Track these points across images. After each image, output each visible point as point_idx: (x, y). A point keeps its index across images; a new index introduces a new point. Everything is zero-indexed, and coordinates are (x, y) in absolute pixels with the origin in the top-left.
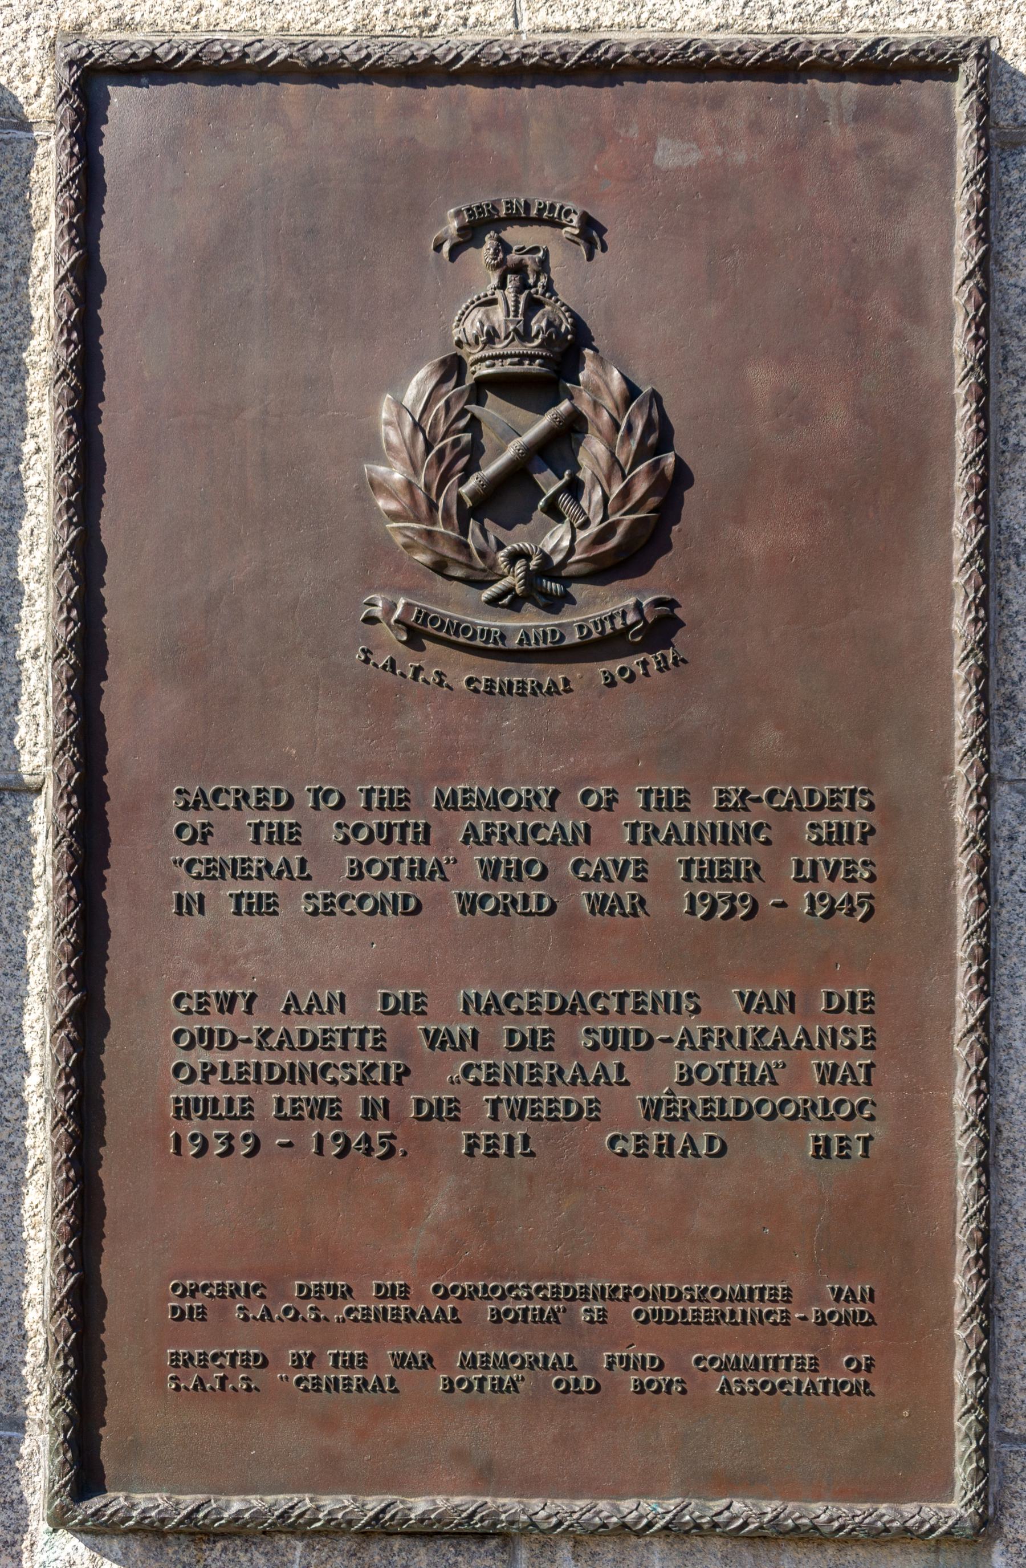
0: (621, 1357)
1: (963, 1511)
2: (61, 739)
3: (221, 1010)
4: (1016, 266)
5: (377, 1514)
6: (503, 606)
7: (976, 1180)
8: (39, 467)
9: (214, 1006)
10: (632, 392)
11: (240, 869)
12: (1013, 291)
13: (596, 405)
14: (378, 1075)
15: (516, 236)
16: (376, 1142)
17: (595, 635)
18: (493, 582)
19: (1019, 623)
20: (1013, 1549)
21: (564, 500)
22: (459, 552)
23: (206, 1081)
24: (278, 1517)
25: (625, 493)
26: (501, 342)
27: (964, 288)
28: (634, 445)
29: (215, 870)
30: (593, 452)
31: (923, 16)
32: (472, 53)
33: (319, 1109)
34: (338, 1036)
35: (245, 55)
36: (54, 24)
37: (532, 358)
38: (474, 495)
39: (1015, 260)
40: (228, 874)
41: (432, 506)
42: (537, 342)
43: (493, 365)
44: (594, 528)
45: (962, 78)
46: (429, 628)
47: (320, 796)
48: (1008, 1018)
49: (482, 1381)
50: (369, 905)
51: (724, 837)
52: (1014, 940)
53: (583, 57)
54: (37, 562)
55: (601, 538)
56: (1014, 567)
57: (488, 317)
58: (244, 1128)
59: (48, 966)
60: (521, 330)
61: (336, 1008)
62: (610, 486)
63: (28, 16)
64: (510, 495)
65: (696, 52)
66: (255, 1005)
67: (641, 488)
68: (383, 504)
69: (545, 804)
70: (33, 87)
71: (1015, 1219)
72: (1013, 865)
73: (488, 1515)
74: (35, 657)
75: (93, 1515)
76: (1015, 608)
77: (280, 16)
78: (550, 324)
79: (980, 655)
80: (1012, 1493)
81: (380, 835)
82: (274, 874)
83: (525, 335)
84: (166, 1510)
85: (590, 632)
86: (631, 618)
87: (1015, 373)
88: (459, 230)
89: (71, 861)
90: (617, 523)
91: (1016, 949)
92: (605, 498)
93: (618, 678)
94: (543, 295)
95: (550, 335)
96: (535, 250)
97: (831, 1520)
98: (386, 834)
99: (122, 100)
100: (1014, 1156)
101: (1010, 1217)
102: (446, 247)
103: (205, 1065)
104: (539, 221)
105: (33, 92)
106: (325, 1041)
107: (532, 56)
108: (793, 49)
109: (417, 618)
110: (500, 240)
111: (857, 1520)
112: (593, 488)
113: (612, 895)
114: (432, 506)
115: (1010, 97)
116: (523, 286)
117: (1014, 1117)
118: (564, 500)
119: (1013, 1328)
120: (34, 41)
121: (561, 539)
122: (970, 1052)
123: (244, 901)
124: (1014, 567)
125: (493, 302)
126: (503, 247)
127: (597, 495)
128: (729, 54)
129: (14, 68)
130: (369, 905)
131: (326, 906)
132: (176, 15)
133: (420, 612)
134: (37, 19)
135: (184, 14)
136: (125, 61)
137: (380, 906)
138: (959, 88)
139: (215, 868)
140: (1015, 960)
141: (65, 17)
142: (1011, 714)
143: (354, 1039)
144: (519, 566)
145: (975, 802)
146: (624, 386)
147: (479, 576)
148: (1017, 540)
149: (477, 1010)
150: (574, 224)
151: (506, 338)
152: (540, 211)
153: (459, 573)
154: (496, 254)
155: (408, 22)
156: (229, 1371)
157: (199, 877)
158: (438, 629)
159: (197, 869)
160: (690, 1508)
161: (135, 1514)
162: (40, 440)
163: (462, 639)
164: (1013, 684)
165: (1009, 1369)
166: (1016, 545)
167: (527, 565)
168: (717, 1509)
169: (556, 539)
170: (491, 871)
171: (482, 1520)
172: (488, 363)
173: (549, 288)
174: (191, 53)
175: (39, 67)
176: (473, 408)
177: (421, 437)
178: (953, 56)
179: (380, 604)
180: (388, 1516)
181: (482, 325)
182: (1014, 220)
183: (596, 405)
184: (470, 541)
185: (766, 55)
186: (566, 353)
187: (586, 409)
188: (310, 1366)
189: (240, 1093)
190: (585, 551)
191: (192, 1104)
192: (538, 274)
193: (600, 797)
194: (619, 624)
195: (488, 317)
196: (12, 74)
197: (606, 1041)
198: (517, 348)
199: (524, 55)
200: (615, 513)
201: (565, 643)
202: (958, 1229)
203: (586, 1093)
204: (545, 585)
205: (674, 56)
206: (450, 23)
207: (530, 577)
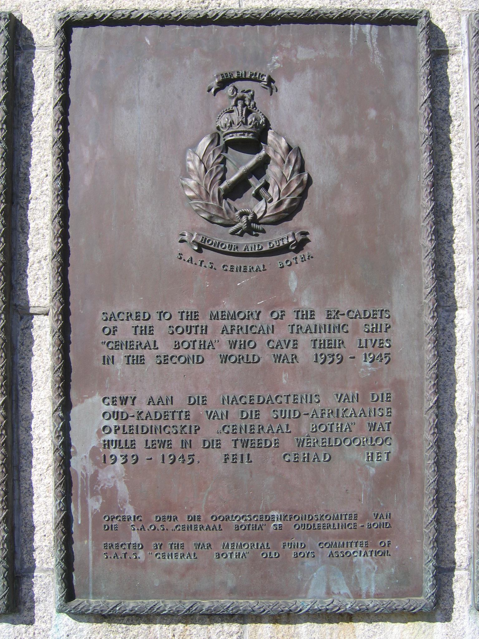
0: (289, 543)
1: (427, 601)
2: (55, 292)
3: (122, 404)
4: (440, 101)
5: (190, 608)
6: (237, 235)
7: (433, 469)
8: (47, 183)
9: (119, 402)
10: (289, 148)
11: (129, 345)
12: (439, 111)
13: (275, 152)
14: (187, 430)
15: (238, 84)
16: (186, 457)
17: (275, 247)
18: (233, 225)
19: (445, 243)
20: (444, 612)
21: (262, 191)
22: (219, 213)
23: (116, 433)
24: (149, 609)
25: (288, 187)
26: (236, 126)
27: (423, 107)
28: (291, 168)
29: (118, 345)
30: (273, 171)
31: (401, 5)
32: (110, 14)
33: (162, 444)
34: (171, 414)
35: (131, 15)
36: (55, 8)
37: (249, 132)
38: (226, 190)
39: (440, 99)
40: (124, 347)
41: (208, 194)
42: (251, 126)
43: (232, 136)
44: (275, 202)
45: (419, 25)
46: (206, 244)
47: (162, 314)
48: (443, 402)
49: (231, 554)
50: (183, 359)
51: (329, 329)
52: (445, 371)
53: (268, 15)
54: (46, 221)
55: (280, 204)
56: (443, 220)
57: (231, 117)
58: (130, 452)
59: (52, 386)
60: (244, 121)
61: (169, 403)
62: (281, 185)
63: (45, 5)
64: (237, 190)
65: (313, 13)
66: (136, 401)
67: (295, 185)
68: (189, 194)
69: (256, 317)
70: (46, 32)
71: (445, 483)
72: (444, 341)
73: (235, 608)
74: (45, 260)
75: (74, 608)
76: (443, 237)
77: (145, 3)
78: (256, 119)
79: (434, 254)
80: (443, 591)
81: (187, 331)
82: (143, 347)
83: (246, 123)
84: (103, 607)
85: (273, 245)
86: (290, 240)
87: (441, 143)
88: (218, 83)
89: (59, 343)
90: (285, 200)
91: (446, 375)
92: (279, 191)
93: (285, 264)
94: (253, 108)
95: (256, 123)
96: (249, 91)
97: (374, 606)
98: (188, 330)
99: (78, 33)
100: (445, 458)
101: (443, 482)
102: (213, 90)
103: (116, 426)
104: (250, 79)
105: (46, 35)
106: (165, 416)
107: (247, 15)
108: (352, 12)
109: (202, 240)
110: (234, 87)
111: (384, 606)
112: (275, 185)
113: (283, 355)
114: (208, 194)
115: (436, 36)
116: (244, 105)
117: (445, 442)
118: (262, 191)
119: (444, 526)
120: (47, 15)
121: (262, 207)
122: (430, 417)
123: (131, 358)
124: (443, 220)
125: (232, 111)
126: (235, 89)
127: (276, 189)
128: (326, 14)
129: (39, 25)
130: (183, 359)
131: (165, 360)
132: (104, 4)
133: (203, 238)
134: (49, 6)
135: (107, 3)
136: (82, 19)
137: (187, 360)
138: (418, 28)
139: (118, 345)
140: (445, 379)
141: (60, 5)
142: (442, 279)
143: (177, 415)
144: (244, 219)
145: (432, 314)
146: (286, 144)
147: (227, 222)
148: (443, 210)
149: (228, 403)
150: (265, 80)
151: (238, 125)
152: (251, 75)
153: (220, 221)
154: (233, 92)
155: (197, 5)
156: (127, 550)
157: (112, 349)
158: (210, 245)
159: (111, 345)
160: (317, 603)
161: (91, 608)
162: (48, 171)
163: (220, 248)
164: (444, 267)
165: (442, 542)
166: (443, 211)
167: (247, 218)
168: (328, 603)
169: (259, 208)
170: (233, 345)
171: (232, 610)
172: (231, 135)
173: (255, 106)
174: (109, 14)
175: (49, 25)
176: (224, 154)
177: (203, 165)
178: (416, 16)
179: (187, 235)
180: (194, 609)
181: (228, 120)
182: (439, 84)
183: (275, 152)
184: (223, 208)
185: (341, 15)
186: (261, 133)
187: (271, 154)
188: (160, 548)
189: (129, 437)
190: (271, 212)
191: (110, 442)
192: (250, 101)
193: (278, 314)
194: (286, 243)
195: (231, 117)
196: (38, 28)
197: (281, 415)
198: (242, 128)
199: (244, 14)
200: (284, 195)
201: (263, 250)
202: (425, 489)
203: (274, 436)
204: (253, 226)
205: (304, 15)
206: (213, 6)
207: (249, 222)
